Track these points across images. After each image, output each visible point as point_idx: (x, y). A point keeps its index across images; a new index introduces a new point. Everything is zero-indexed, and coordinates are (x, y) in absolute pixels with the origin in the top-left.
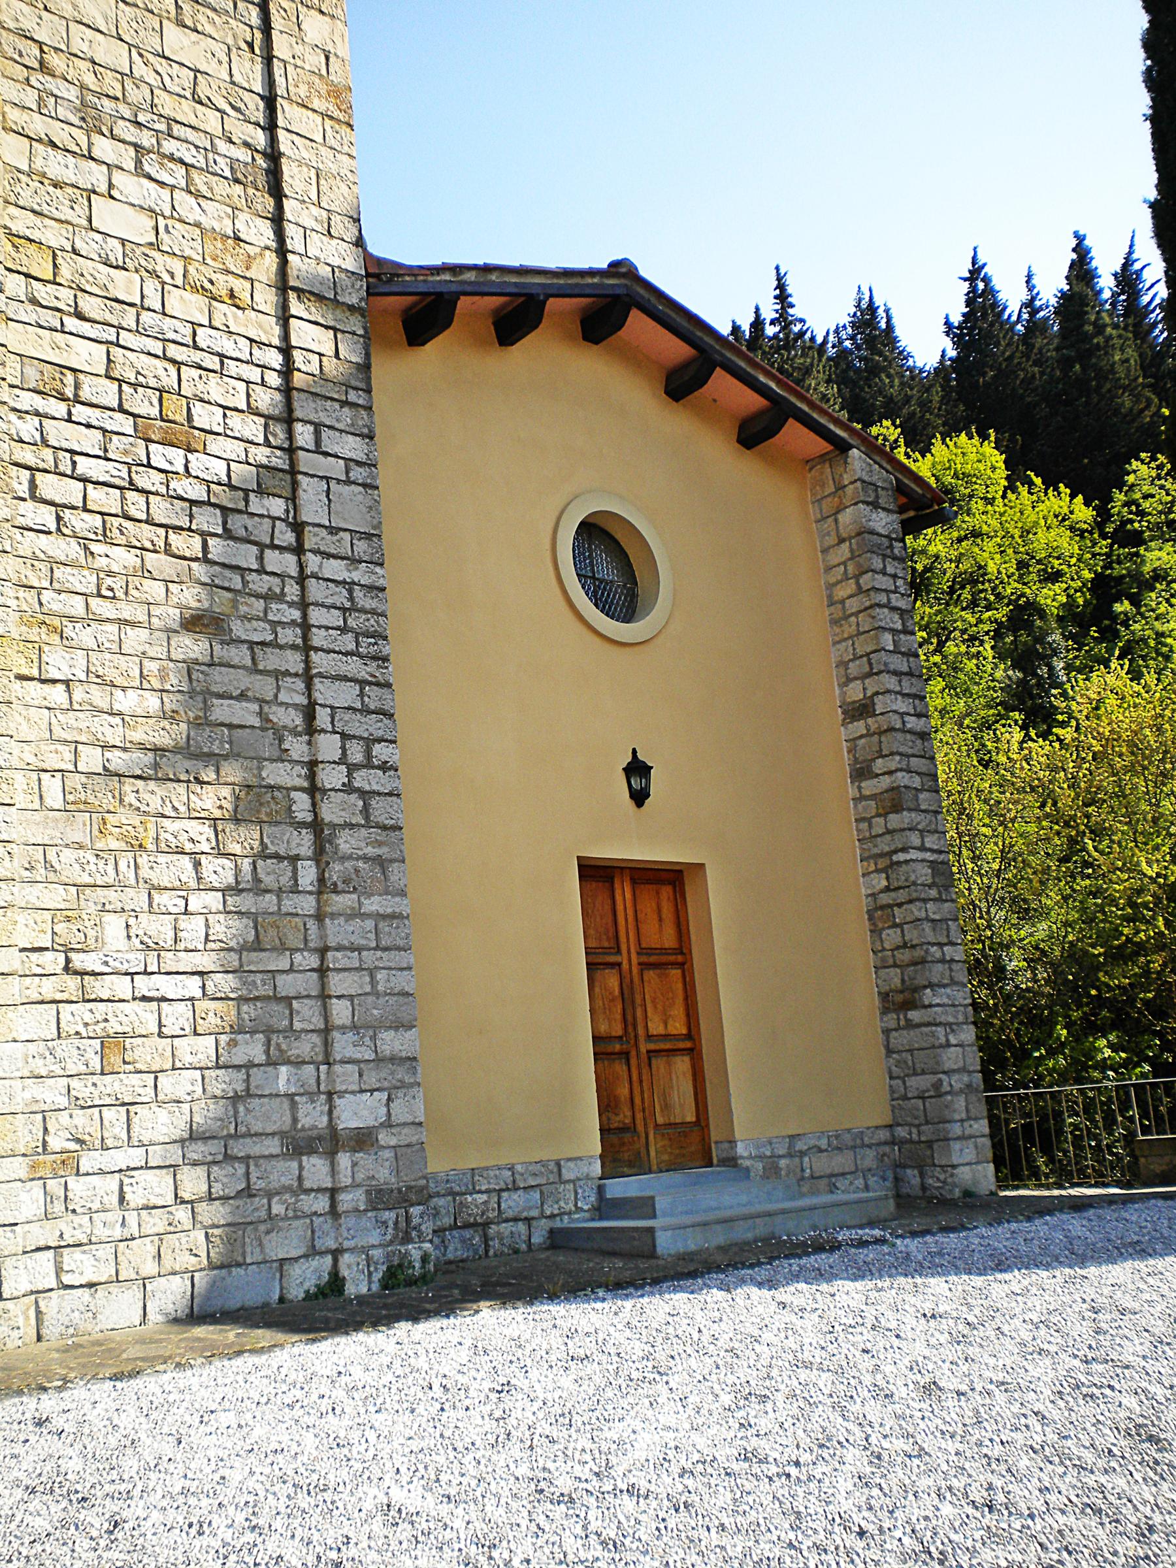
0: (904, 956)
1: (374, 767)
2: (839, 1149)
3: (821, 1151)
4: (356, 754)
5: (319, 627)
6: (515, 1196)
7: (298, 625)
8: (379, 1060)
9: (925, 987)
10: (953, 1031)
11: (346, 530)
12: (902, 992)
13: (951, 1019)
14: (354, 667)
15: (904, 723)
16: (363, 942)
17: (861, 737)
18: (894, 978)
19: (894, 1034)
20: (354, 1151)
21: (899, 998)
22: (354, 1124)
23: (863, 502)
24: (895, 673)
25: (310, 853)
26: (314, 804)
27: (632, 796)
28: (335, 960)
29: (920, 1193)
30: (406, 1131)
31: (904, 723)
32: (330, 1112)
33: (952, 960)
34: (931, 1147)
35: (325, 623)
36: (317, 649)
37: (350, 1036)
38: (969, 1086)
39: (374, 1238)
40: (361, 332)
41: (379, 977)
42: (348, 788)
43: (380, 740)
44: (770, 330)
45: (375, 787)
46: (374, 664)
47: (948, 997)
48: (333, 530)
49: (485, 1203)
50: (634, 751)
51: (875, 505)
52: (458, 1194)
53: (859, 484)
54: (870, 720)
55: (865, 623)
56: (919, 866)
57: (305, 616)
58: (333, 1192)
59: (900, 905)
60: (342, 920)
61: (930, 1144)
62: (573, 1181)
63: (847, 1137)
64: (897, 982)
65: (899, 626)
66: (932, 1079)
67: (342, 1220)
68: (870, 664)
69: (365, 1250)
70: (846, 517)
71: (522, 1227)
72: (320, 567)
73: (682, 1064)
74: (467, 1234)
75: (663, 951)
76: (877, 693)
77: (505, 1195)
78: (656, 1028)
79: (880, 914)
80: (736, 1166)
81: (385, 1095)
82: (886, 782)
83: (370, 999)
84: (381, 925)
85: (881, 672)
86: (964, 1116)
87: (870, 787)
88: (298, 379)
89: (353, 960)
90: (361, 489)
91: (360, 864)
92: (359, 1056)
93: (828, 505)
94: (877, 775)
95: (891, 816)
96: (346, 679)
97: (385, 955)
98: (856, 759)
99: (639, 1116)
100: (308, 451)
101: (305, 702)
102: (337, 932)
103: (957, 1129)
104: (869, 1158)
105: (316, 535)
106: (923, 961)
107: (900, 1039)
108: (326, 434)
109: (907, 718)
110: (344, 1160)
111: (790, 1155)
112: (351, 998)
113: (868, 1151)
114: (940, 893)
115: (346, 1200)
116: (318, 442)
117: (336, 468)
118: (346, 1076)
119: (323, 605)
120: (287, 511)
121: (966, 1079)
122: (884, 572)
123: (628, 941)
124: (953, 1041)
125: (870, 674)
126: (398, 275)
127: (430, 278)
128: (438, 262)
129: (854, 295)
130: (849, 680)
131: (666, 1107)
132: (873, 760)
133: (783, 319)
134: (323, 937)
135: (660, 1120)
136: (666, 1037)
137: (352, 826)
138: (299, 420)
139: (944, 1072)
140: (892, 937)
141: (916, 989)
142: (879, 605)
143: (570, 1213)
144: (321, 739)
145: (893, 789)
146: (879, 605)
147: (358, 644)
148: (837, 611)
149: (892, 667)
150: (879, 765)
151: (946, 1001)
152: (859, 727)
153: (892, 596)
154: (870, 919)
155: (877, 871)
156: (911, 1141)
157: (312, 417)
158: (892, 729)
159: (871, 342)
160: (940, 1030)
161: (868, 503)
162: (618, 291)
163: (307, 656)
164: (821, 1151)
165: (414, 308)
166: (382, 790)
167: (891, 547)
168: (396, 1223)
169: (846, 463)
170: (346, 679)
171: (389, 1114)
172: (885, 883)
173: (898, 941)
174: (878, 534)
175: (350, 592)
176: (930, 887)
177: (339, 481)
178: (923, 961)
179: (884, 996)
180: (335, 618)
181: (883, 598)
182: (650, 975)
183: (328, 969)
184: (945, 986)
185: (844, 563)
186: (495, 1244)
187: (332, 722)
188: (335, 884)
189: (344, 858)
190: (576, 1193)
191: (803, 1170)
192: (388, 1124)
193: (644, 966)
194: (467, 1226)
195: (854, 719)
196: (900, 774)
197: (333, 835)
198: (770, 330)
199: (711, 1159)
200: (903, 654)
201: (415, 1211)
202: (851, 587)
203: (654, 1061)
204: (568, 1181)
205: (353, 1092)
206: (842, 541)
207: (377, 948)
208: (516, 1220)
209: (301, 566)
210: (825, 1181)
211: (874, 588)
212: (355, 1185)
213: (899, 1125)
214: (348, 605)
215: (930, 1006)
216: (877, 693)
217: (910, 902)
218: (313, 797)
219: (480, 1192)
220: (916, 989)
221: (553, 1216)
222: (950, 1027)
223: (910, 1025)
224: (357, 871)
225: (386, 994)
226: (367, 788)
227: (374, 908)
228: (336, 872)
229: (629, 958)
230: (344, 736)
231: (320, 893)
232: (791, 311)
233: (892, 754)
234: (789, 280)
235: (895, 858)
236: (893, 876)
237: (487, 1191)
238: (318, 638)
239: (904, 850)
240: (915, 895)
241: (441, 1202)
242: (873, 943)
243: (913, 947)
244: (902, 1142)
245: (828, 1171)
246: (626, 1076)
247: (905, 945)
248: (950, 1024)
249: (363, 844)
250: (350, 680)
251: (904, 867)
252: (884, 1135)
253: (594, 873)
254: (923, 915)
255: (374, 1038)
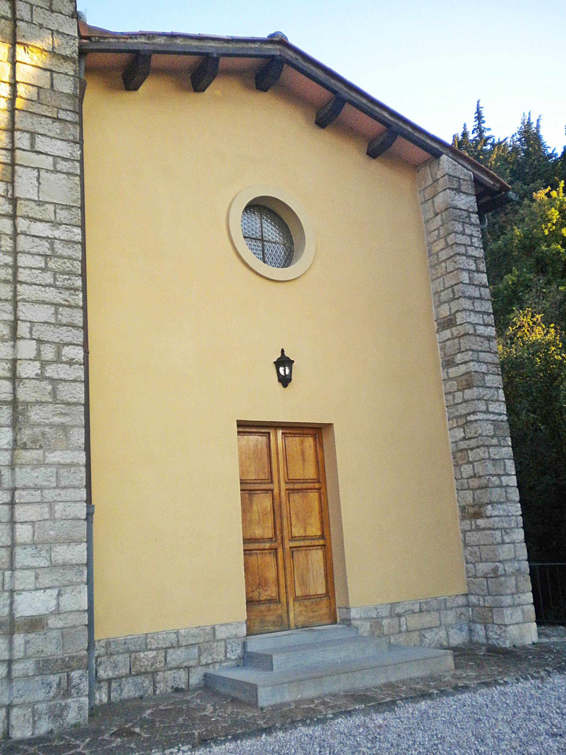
0: (475, 483)
1: (62, 362)
2: (427, 611)
3: (413, 612)
4: (48, 353)
5: (25, 268)
6: (179, 652)
7: (10, 267)
8: (53, 566)
9: (488, 504)
10: (507, 533)
11: (50, 203)
12: (473, 506)
13: (506, 525)
14: (51, 295)
15: (475, 330)
16: (46, 483)
17: (448, 340)
18: (468, 497)
19: (468, 534)
20: (27, 632)
21: (471, 510)
22: (29, 613)
23: (449, 188)
24: (469, 298)
25: (9, 422)
26: (14, 389)
27: (280, 380)
28: (21, 497)
29: (485, 641)
30: (72, 616)
31: (475, 330)
32: (11, 604)
33: (508, 486)
34: (491, 611)
35: (30, 265)
36: (21, 283)
37: (29, 550)
38: (518, 570)
39: (40, 695)
40: (72, 73)
41: (57, 507)
42: (40, 377)
43: (68, 344)
44: (471, 137)
45: (62, 376)
46: (67, 293)
47: (504, 510)
48: (40, 203)
49: (154, 658)
50: (283, 351)
51: (458, 190)
52: (133, 652)
53: (446, 177)
54: (454, 329)
55: (450, 266)
56: (484, 424)
57: (15, 260)
58: (10, 662)
59: (472, 449)
60: (29, 469)
61: (491, 608)
62: (224, 640)
63: (434, 604)
64: (470, 500)
65: (473, 267)
66: (492, 565)
67: (14, 684)
68: (453, 293)
69: (32, 705)
70: (439, 200)
71: (182, 674)
72: (29, 227)
73: (317, 556)
74: (139, 679)
75: (305, 481)
76: (458, 311)
77: (170, 651)
78: (297, 531)
79: (460, 455)
80: (350, 625)
81: (55, 592)
82: (463, 369)
83: (48, 523)
84: (61, 471)
85: (460, 297)
86: (514, 590)
87: (453, 372)
88: (19, 103)
89: (37, 496)
90: (65, 176)
91: (47, 429)
92: (36, 564)
93: (428, 193)
94: (458, 364)
95: (466, 391)
96: (44, 303)
97: (62, 492)
98: (445, 354)
99: (283, 591)
100: (24, 150)
101: (11, 318)
102: (24, 476)
103: (508, 600)
104: (450, 617)
105: (25, 206)
106: (486, 487)
107: (473, 537)
108: (39, 139)
109: (478, 327)
110: (19, 639)
111: (391, 616)
112: (33, 523)
113: (449, 612)
114: (499, 441)
115: (18, 668)
116: (32, 145)
117: (48, 162)
118: (24, 579)
119: (29, 253)
120: (7, 191)
121: (516, 565)
122: (463, 233)
123: (280, 475)
124: (507, 539)
125: (453, 299)
126: (105, 38)
127: (129, 41)
128: (136, 30)
129: (521, 117)
130: (441, 303)
131: (304, 584)
132: (456, 354)
133: (480, 130)
134: (14, 480)
135: (299, 593)
136: (305, 538)
137: (41, 403)
138: (18, 130)
139: (500, 561)
140: (467, 470)
141: (482, 505)
142: (459, 254)
143: (221, 662)
144: (20, 343)
145: (467, 373)
146: (459, 254)
147: (55, 279)
148: (434, 259)
149: (467, 294)
150: (459, 358)
151: (501, 513)
152: (447, 334)
153: (468, 248)
154: (454, 458)
155: (458, 426)
156: (479, 606)
157: (30, 128)
158: (467, 334)
159: (527, 140)
160: (498, 534)
161: (452, 189)
162: (273, 53)
163: (15, 288)
164: (413, 612)
165: (126, 65)
166: (67, 378)
167: (469, 217)
168: (59, 684)
169: (439, 164)
170: (44, 303)
171: (58, 605)
172: (463, 435)
173: (471, 473)
174: (460, 209)
175: (52, 244)
176: (492, 437)
177: (47, 171)
178: (486, 487)
179: (463, 509)
180: (39, 262)
181: (462, 250)
182: (296, 497)
183: (16, 503)
184: (501, 503)
185: (438, 229)
186: (161, 687)
187: (31, 332)
188: (25, 444)
189: (33, 425)
190: (226, 648)
191: (400, 626)
192: (57, 612)
193: (290, 491)
194: (139, 674)
195: (444, 328)
196: (471, 364)
197: (25, 411)
198: (471, 137)
199: (336, 621)
200: (476, 285)
201: (75, 674)
202: (441, 244)
203: (295, 554)
204: (221, 640)
205: (29, 590)
206: (436, 214)
207: (57, 487)
208: (178, 668)
209: (15, 227)
210: (417, 633)
211: (455, 243)
212: (26, 657)
213: (472, 594)
214: (49, 253)
215: (491, 517)
216: (458, 311)
217: (478, 447)
218: (14, 384)
219: (151, 650)
220: (482, 505)
221: (207, 665)
222: (506, 531)
223: (478, 529)
224: (43, 434)
225: (62, 519)
226: (56, 377)
227: (56, 460)
228: (26, 435)
229: (280, 486)
230: (40, 342)
231: (14, 449)
232: (483, 125)
233: (467, 350)
234: (484, 113)
235: (469, 418)
236: (467, 430)
237: (157, 649)
238: (23, 275)
239: (474, 413)
240: (481, 443)
241: (119, 658)
242: (456, 474)
243: (480, 477)
244: (474, 606)
245: (419, 626)
246: (273, 564)
247: (475, 476)
248: (505, 529)
249: (50, 416)
250: (47, 303)
251: (475, 425)
252: (461, 601)
253: (245, 427)
254: (487, 456)
255: (50, 551)
